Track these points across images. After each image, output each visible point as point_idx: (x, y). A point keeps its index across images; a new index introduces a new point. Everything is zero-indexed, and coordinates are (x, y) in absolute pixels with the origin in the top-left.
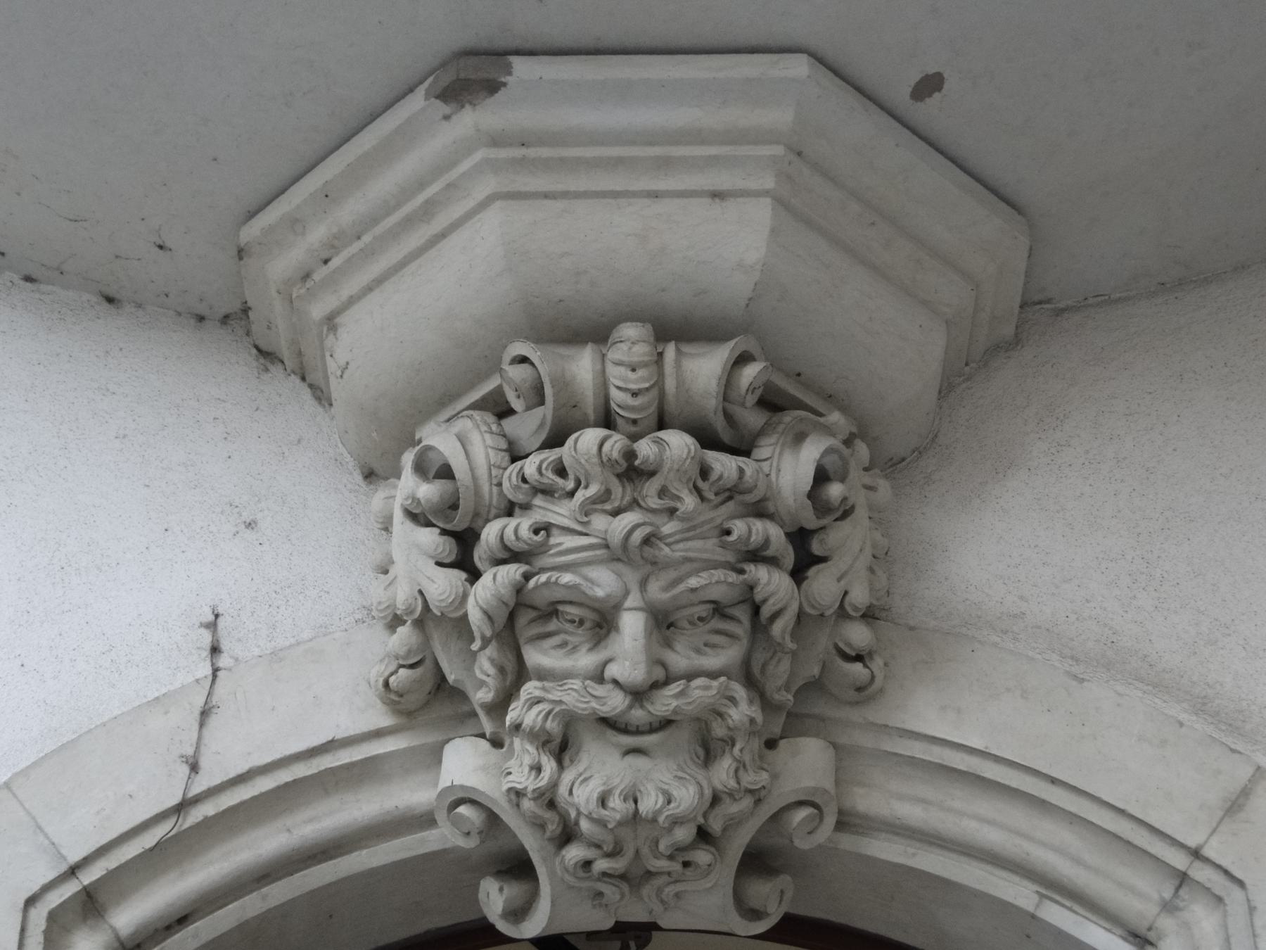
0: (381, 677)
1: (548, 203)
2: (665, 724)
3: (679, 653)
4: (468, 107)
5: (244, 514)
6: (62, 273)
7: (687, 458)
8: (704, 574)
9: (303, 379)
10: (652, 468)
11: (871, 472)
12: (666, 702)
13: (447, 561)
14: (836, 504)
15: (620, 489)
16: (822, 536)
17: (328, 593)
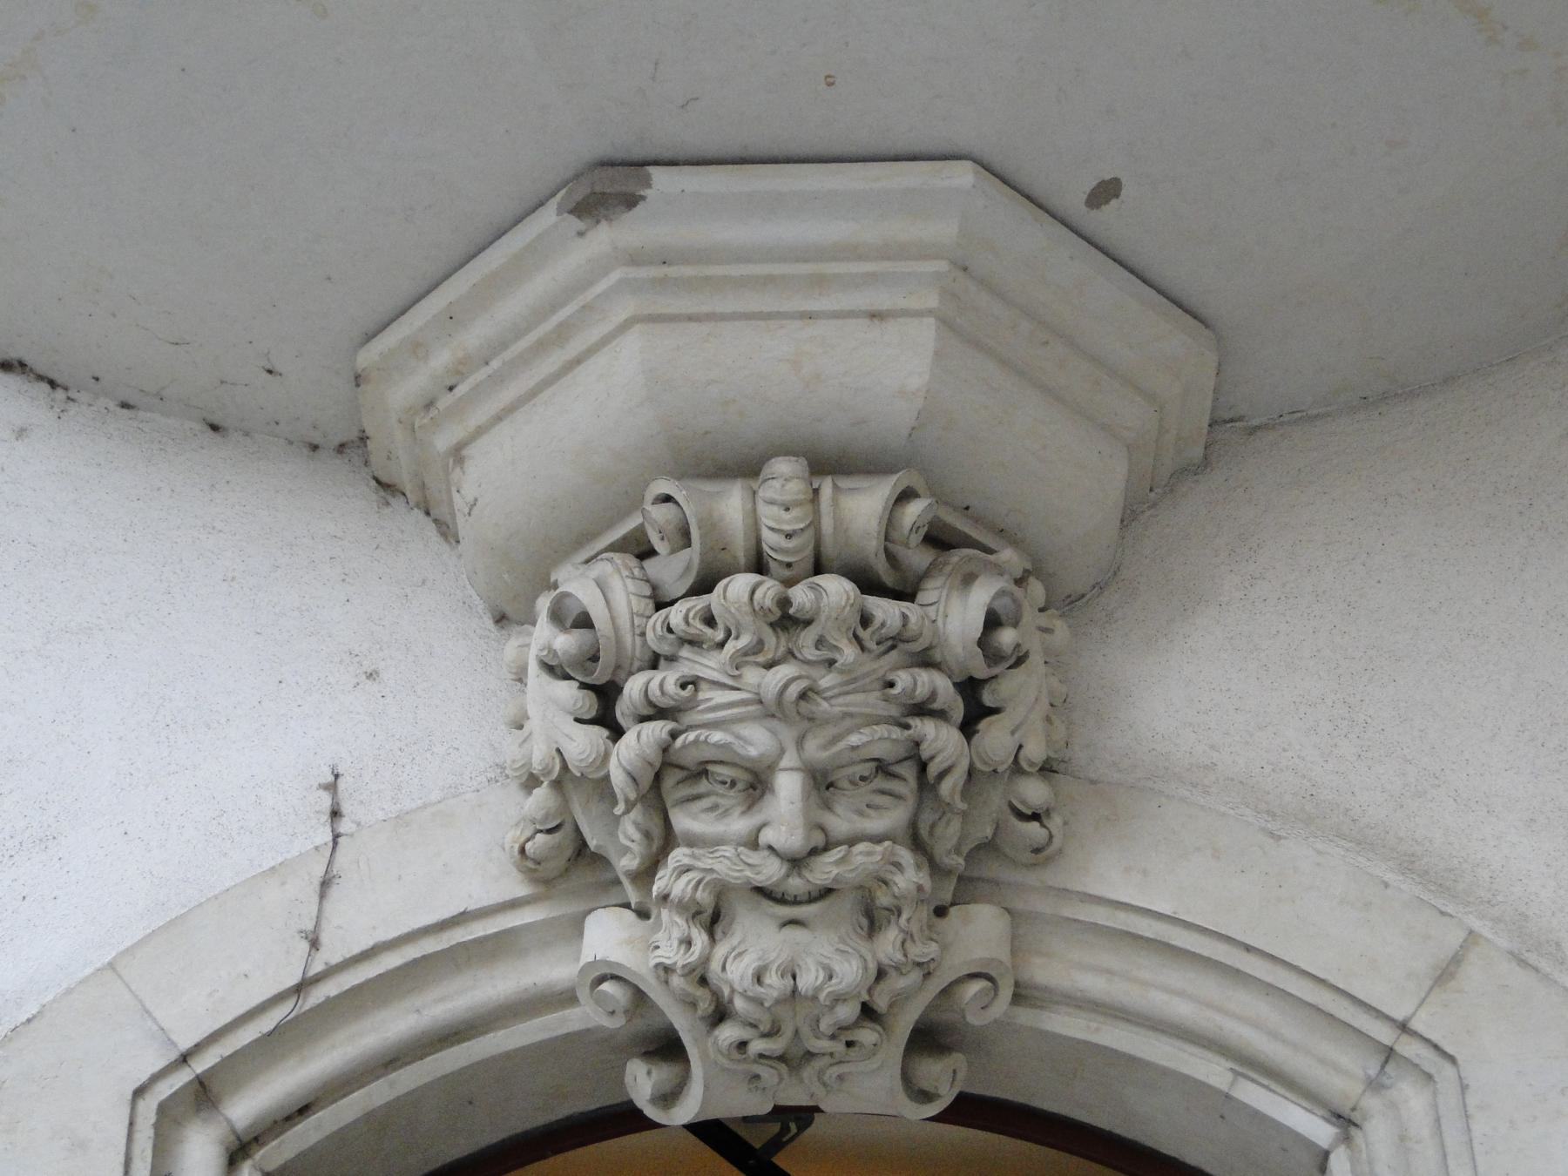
0: (515, 842)
1: (693, 326)
2: (826, 892)
3: (839, 816)
4: (604, 223)
5: (365, 662)
6: (161, 399)
7: (846, 605)
8: (866, 730)
9: (428, 513)
10: (807, 617)
11: (1049, 612)
12: (825, 870)
13: (587, 717)
14: (1009, 651)
15: (774, 639)
16: (993, 685)
17: (458, 749)
